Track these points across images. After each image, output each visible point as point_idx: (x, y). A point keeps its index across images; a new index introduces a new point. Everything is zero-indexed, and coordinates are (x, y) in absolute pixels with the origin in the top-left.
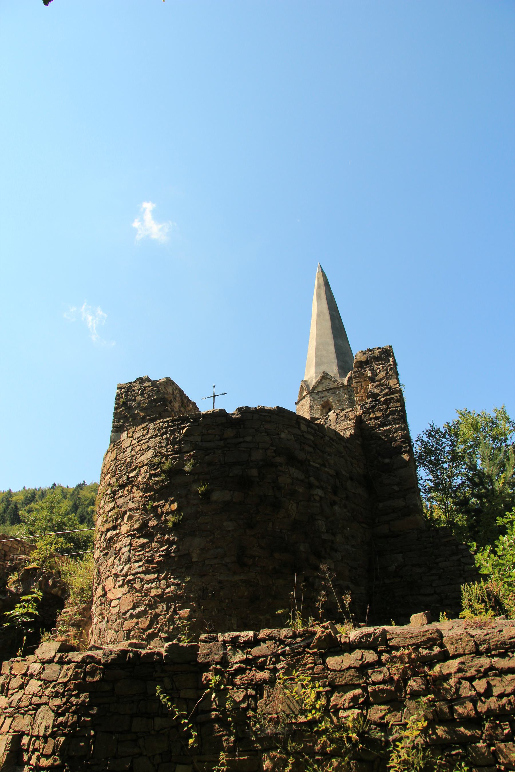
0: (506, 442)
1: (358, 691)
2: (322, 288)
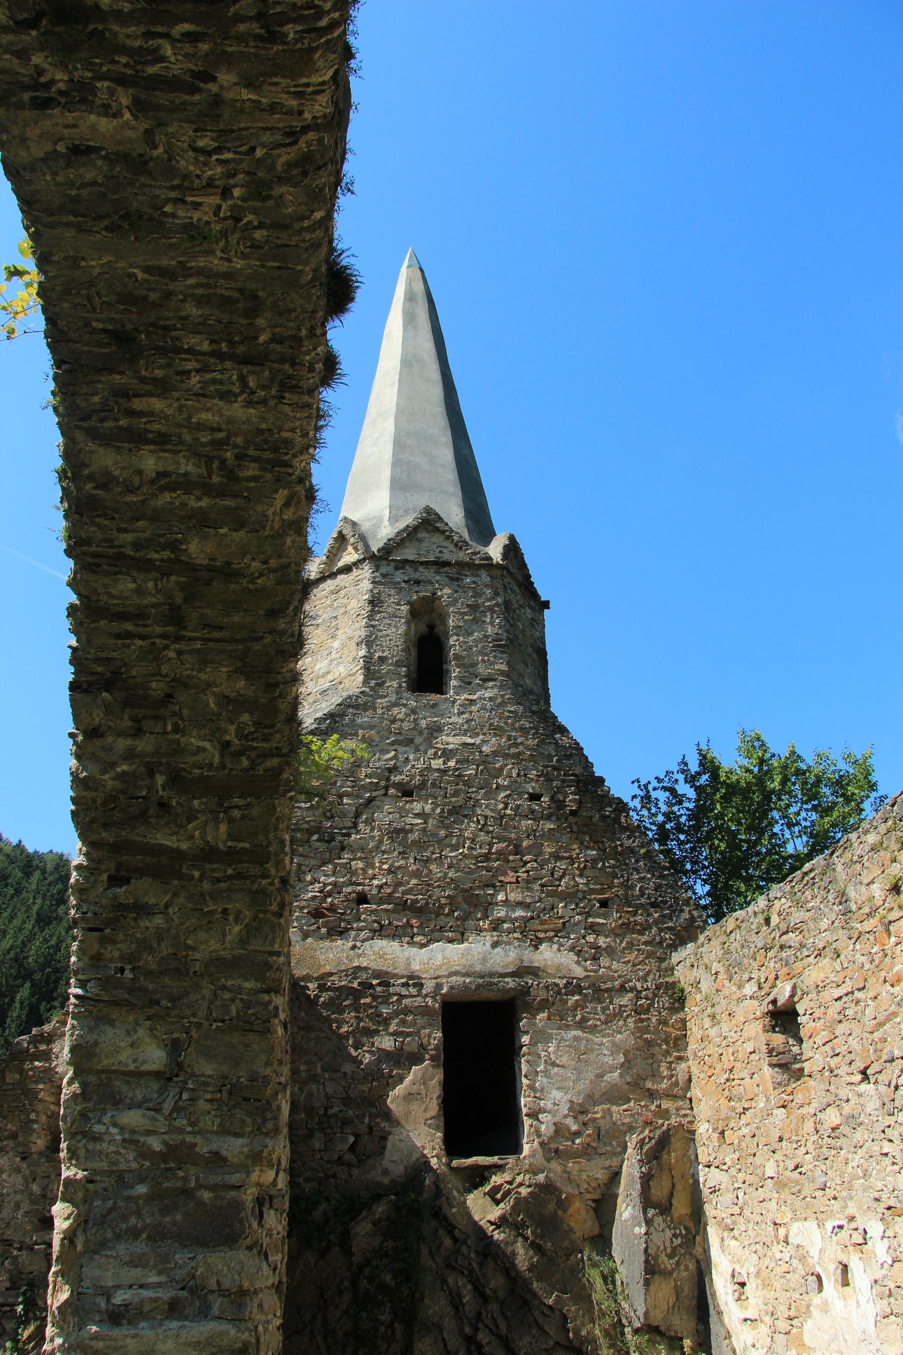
1: (370, 699)
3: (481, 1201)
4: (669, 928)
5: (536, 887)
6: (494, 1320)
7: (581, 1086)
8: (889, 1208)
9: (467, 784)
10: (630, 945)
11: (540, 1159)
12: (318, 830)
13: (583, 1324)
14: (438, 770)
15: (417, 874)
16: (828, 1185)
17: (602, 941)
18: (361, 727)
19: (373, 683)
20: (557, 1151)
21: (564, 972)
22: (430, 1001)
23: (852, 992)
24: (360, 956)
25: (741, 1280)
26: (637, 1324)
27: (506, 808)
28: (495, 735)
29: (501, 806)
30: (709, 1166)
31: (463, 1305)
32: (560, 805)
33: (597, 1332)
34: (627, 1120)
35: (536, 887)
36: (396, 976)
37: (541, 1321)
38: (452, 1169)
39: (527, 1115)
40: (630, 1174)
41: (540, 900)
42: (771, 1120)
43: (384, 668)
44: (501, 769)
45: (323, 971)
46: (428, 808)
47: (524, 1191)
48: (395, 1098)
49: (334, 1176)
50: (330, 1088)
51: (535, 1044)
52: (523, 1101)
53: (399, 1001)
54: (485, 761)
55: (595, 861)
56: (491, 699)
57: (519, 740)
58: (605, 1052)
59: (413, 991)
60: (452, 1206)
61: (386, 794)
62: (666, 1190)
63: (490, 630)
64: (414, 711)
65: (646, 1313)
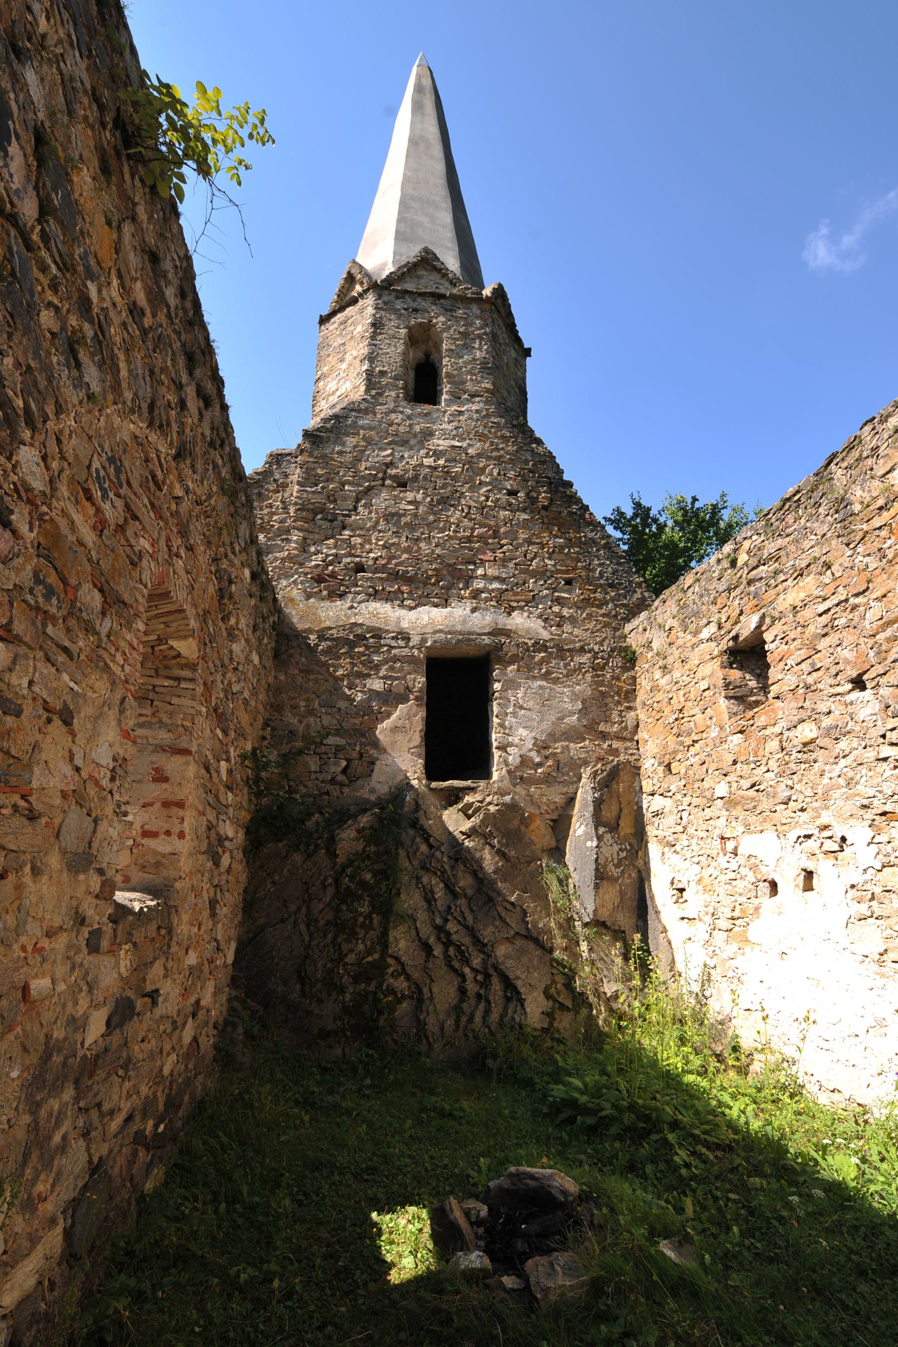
0: (364, 851)
2: (428, 95)
3: (455, 816)
4: (623, 605)
5: (511, 565)
6: (463, 913)
7: (545, 726)
8: (884, 814)
9: (453, 478)
10: (590, 616)
11: (507, 783)
12: (323, 510)
13: (541, 918)
14: (429, 467)
15: (408, 550)
16: (794, 798)
17: (566, 612)
18: (363, 428)
19: (373, 392)
20: (521, 778)
21: (533, 635)
22: (416, 652)
23: (846, 600)
24: (356, 614)
25: (680, 886)
26: (587, 920)
27: (487, 500)
28: (480, 440)
29: (483, 498)
30: (653, 795)
31: (435, 900)
32: (534, 501)
33: (552, 924)
34: (583, 756)
35: (511, 565)
36: (388, 632)
37: (503, 915)
38: (431, 789)
39: (497, 748)
40: (584, 799)
41: (514, 576)
42: (725, 746)
43: (384, 381)
44: (484, 468)
45: (323, 625)
46: (419, 497)
47: (492, 809)
48: (382, 730)
49: (328, 793)
50: (326, 720)
51: (506, 690)
52: (494, 736)
53: (389, 651)
54: (470, 461)
55: (562, 548)
56: (477, 411)
57: (501, 446)
58: (566, 700)
59: (401, 643)
60: (428, 819)
61: (383, 485)
62: (614, 813)
63: (478, 354)
64: (409, 418)
65: (595, 911)
